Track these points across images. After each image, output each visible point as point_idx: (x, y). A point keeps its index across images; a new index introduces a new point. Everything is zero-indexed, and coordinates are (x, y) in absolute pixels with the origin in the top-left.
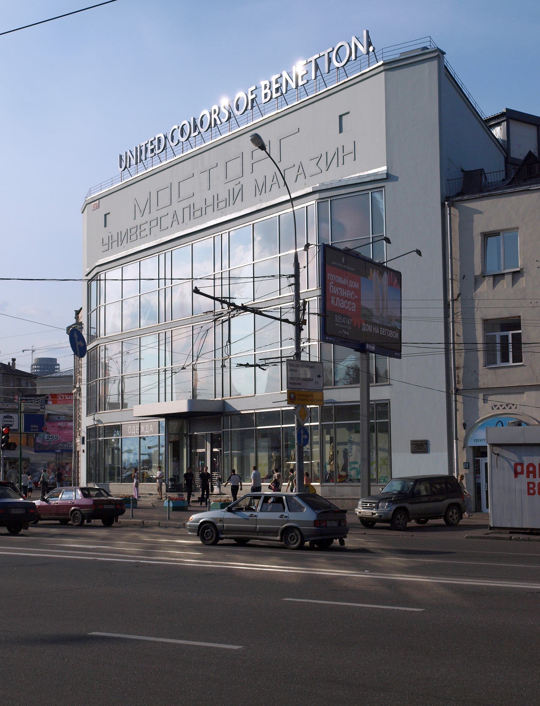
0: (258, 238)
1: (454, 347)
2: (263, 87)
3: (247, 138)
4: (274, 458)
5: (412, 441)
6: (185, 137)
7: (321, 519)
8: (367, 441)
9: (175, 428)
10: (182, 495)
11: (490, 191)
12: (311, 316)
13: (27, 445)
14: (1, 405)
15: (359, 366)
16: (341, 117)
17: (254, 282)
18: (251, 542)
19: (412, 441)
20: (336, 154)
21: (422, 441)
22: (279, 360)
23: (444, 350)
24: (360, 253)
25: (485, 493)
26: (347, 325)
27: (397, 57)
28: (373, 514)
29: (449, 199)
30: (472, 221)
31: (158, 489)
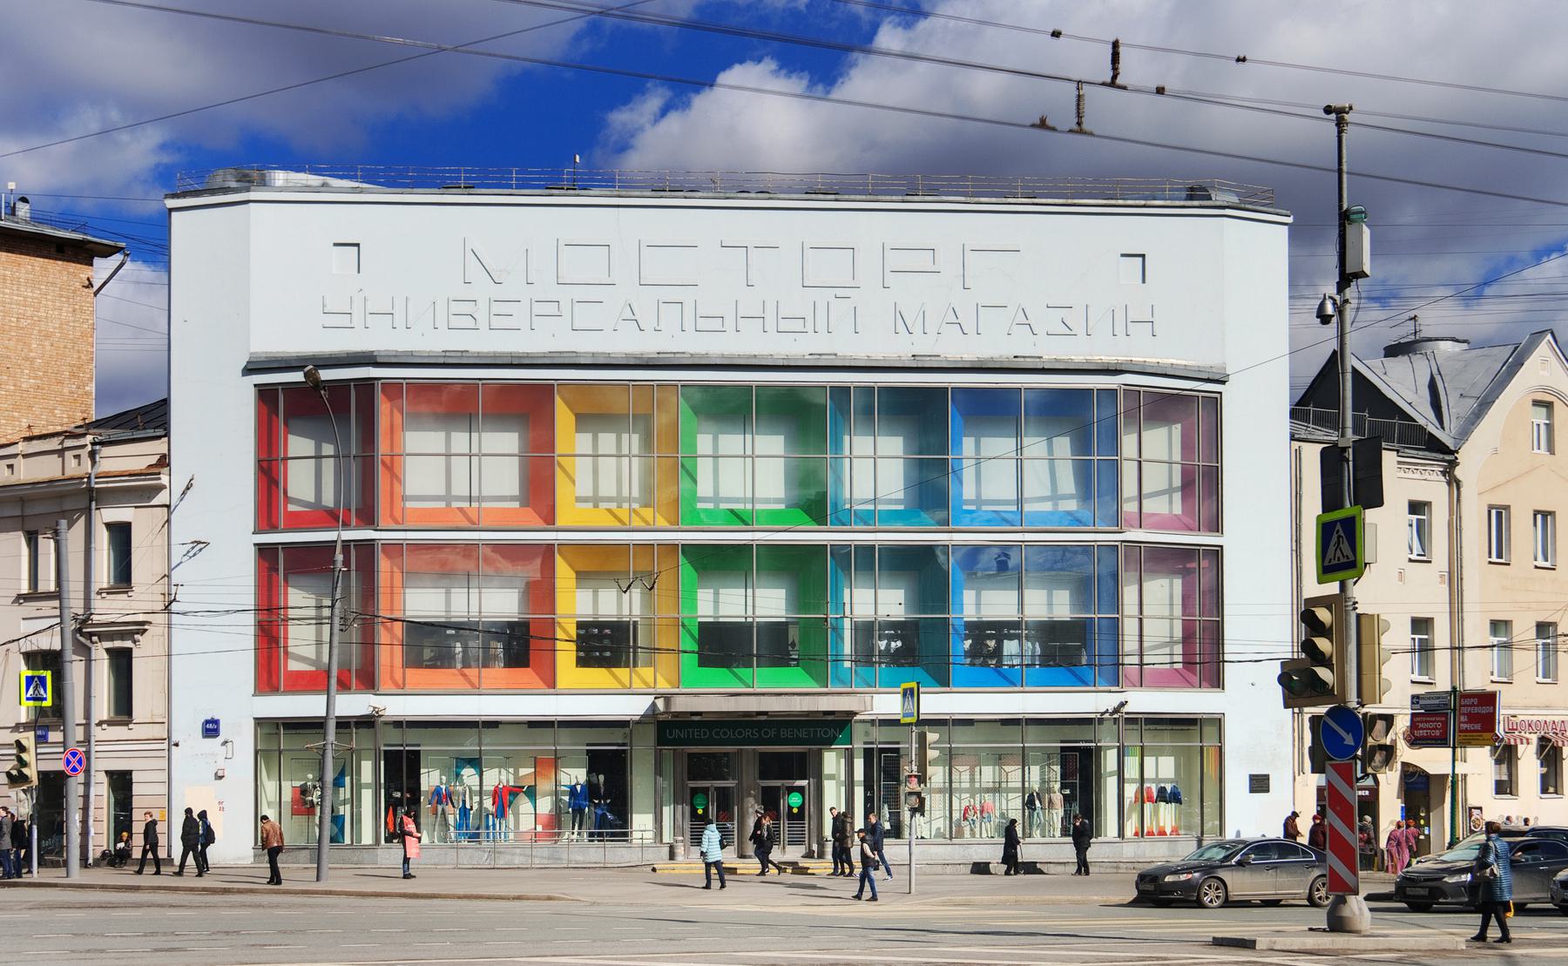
0: (661, 27)
1: (1171, 610)
2: (1398, 636)
3: (284, 886)
4: (1421, 865)
5: (1252, 791)
6: (917, 330)
7: (829, 849)
8: (48, 912)
9: (863, 470)
10: (866, 631)
11: (868, 786)
12: (1167, 613)
13: (1546, 514)
14: (7, 472)
15: (298, 784)
16: (358, 245)
17: (1141, 655)
18: (1476, 701)
19: (1252, 791)
20: (469, 48)
21: (258, 481)
22: (749, 452)
23: (625, 436)
24: (775, 73)
25: (1269, 892)
26: (331, 618)
27: (1446, 587)
28: (793, 645)
29: (165, 403)
30: (1482, 746)
31: (1187, 486)
